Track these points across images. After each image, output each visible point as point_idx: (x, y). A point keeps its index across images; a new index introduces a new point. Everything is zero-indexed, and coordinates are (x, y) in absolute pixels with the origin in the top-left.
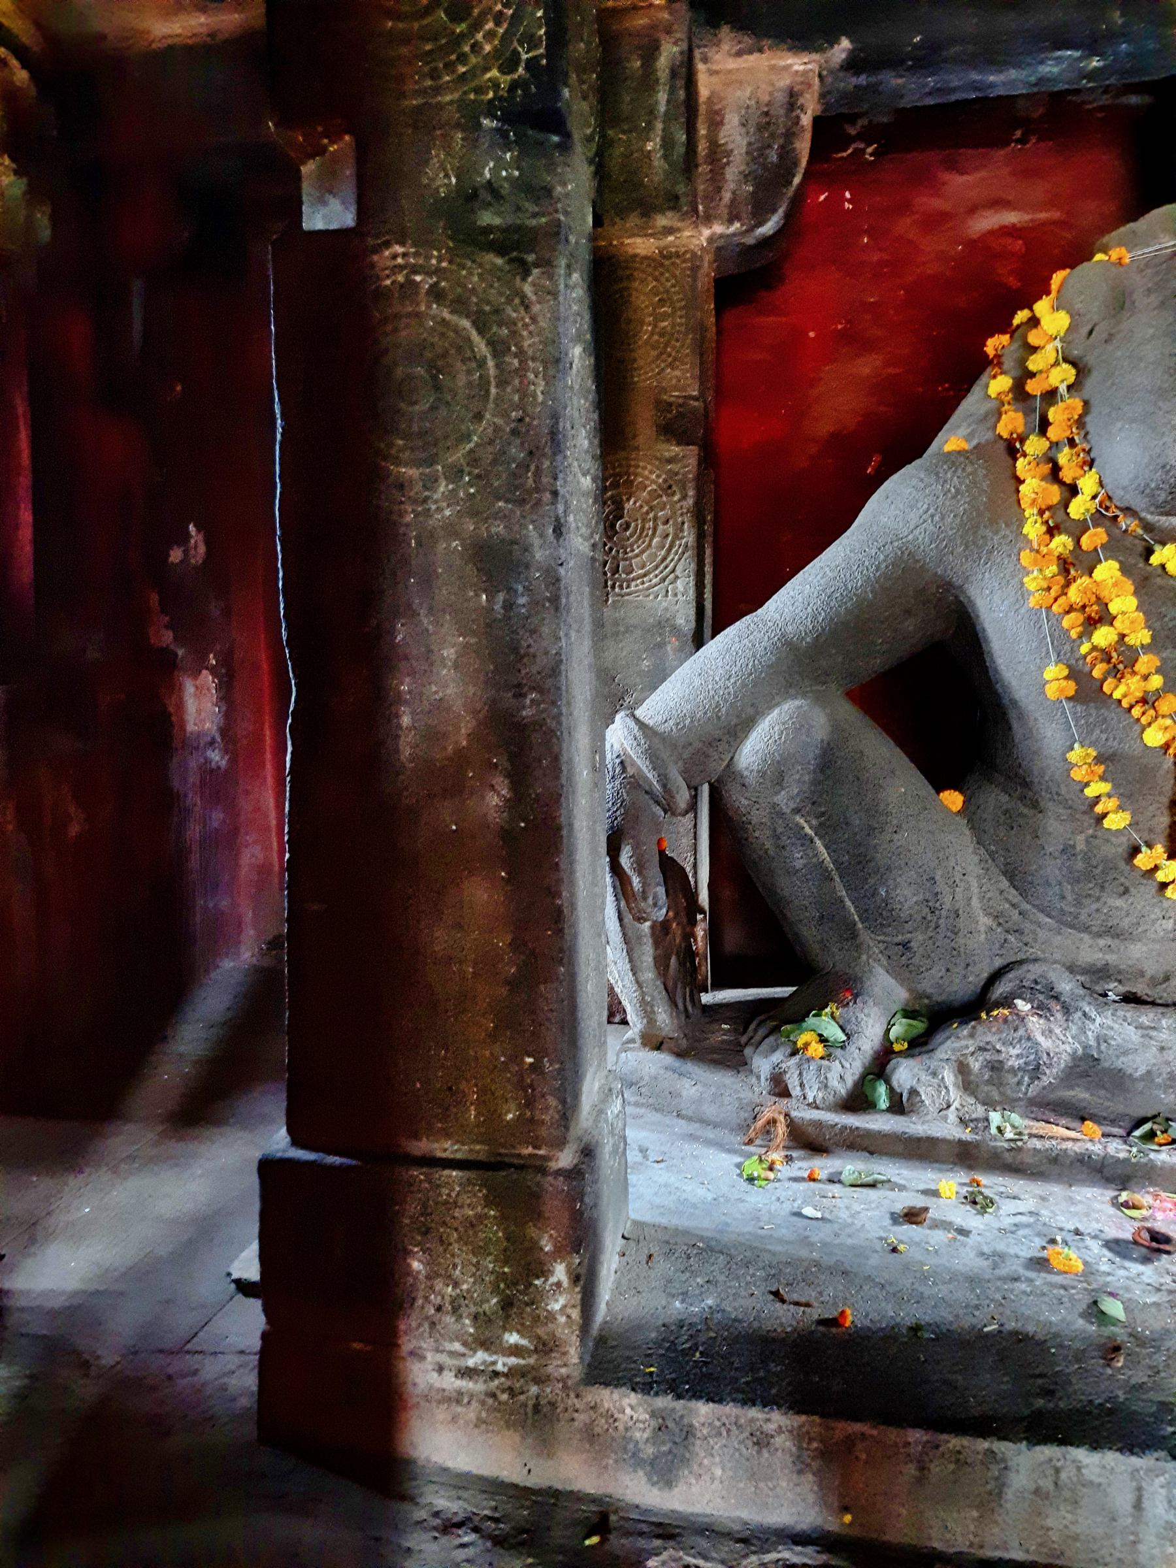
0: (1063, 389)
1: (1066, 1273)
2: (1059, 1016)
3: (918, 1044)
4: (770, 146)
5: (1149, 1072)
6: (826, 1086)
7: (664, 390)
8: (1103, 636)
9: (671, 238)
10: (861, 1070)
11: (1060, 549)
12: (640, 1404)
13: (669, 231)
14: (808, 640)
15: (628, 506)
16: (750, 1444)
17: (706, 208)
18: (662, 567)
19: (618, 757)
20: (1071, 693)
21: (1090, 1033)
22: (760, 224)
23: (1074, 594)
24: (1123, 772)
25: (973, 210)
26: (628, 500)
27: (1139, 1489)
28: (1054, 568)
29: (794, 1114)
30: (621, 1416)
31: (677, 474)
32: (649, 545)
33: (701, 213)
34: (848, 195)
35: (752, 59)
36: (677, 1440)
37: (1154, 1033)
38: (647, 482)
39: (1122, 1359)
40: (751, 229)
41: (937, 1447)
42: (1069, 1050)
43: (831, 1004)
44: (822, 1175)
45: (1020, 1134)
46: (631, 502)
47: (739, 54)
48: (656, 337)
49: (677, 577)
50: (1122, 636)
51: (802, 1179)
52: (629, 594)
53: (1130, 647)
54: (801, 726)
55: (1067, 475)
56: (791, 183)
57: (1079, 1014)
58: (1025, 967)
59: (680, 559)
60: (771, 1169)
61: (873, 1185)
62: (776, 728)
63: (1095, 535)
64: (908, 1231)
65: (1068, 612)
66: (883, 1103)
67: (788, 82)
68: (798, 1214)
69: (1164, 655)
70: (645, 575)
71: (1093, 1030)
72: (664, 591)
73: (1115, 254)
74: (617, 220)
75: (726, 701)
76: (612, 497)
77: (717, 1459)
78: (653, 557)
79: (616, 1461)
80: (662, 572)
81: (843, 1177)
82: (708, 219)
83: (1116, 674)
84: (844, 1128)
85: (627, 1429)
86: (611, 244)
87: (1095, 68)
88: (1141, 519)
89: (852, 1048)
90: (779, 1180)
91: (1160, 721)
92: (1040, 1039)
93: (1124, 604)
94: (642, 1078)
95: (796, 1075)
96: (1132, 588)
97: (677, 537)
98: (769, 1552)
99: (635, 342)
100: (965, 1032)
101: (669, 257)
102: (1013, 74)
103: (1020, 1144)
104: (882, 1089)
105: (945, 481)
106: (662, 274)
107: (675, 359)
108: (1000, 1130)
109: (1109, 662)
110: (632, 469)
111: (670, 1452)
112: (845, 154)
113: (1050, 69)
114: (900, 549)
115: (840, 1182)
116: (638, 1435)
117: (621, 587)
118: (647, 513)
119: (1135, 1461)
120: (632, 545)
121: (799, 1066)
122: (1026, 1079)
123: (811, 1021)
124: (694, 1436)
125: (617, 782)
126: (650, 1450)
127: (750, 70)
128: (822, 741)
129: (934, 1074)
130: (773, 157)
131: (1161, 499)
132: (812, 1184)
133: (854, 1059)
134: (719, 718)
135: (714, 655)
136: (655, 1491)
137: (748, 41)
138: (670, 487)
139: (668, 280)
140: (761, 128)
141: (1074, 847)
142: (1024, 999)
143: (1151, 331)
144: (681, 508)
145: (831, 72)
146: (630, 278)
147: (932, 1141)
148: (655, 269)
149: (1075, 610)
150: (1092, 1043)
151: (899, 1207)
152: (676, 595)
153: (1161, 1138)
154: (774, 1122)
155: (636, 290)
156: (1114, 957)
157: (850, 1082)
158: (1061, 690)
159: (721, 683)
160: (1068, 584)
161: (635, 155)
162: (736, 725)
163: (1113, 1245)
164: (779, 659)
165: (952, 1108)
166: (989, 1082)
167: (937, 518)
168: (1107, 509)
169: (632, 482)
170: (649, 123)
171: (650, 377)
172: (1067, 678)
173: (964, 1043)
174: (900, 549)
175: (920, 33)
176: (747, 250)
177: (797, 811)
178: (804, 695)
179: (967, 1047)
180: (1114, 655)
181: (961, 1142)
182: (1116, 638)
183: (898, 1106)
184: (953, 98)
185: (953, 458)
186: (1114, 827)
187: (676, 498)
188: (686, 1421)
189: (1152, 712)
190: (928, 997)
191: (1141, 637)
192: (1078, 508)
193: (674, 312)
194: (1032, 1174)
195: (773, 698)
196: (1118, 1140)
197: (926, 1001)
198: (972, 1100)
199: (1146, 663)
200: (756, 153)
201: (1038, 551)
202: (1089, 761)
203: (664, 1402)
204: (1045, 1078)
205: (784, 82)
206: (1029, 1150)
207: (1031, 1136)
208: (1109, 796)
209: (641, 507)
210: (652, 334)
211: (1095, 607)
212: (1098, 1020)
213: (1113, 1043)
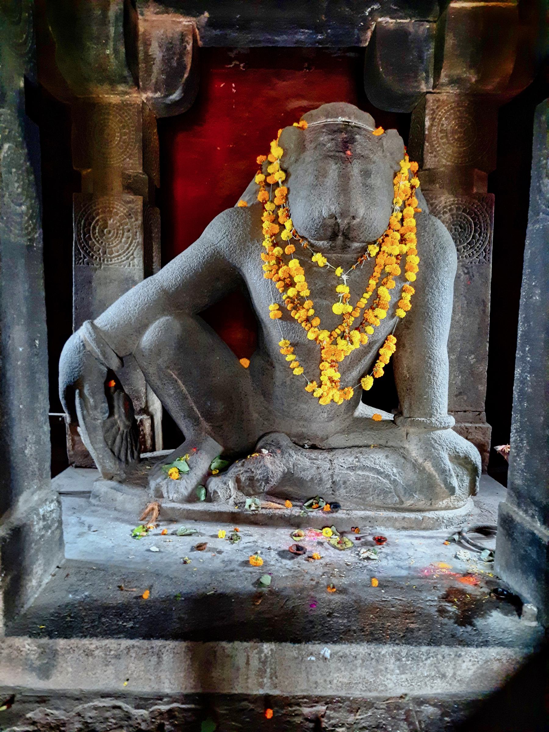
0: (280, 183)
1: (255, 566)
2: (279, 455)
3: (223, 470)
4: (173, 58)
5: (312, 478)
6: (178, 492)
7: (126, 169)
8: (291, 292)
9: (127, 97)
10: (196, 483)
11: (277, 253)
12: (32, 643)
13: (126, 93)
14: (173, 289)
15: (110, 222)
16: (83, 655)
17: (143, 84)
18: (127, 252)
19: (82, 342)
20: (280, 316)
21: (291, 463)
22: (171, 94)
23: (281, 274)
24: (301, 350)
25: (288, 97)
26: (110, 220)
27: (248, 656)
28: (274, 262)
29: (163, 505)
30: (24, 649)
31: (133, 209)
32: (121, 242)
33: (141, 86)
34: (233, 85)
35: (164, 17)
36: (51, 657)
37: (315, 461)
38: (118, 212)
39: (260, 601)
40: (167, 96)
41: (165, 647)
42: (282, 470)
43: (188, 455)
44: (170, 532)
45: (258, 507)
46: (112, 221)
47: (157, 13)
48: (121, 143)
49: (134, 258)
50: (299, 292)
51: (160, 534)
52: (111, 264)
53: (302, 297)
54: (167, 329)
55: (281, 220)
56: (183, 76)
57: (287, 454)
58: (270, 435)
59: (135, 249)
60: (147, 531)
61: (190, 535)
62: (157, 330)
63: (290, 247)
64: (197, 554)
65: (278, 281)
66: (203, 498)
67: (181, 29)
68: (149, 550)
69: (315, 301)
70: (119, 256)
71: (292, 461)
72: (128, 264)
73: (301, 124)
74: (99, 85)
75: (134, 316)
76: (102, 218)
77: (69, 664)
78: (122, 247)
79: (23, 670)
80: (127, 255)
81: (177, 532)
82: (145, 90)
83: (295, 308)
84: (184, 510)
85: (27, 654)
86: (98, 97)
87: (320, 39)
88: (309, 242)
89: (192, 474)
90: (148, 536)
91: (312, 329)
92: (269, 466)
93: (300, 278)
94: (101, 494)
95: (165, 488)
96: (303, 273)
97: (133, 239)
98: (89, 702)
99: (111, 145)
100: (240, 464)
101: (127, 105)
102: (285, 37)
103: (257, 512)
104: (203, 491)
105: (233, 220)
106: (123, 113)
107: (131, 154)
108: (250, 506)
109: (294, 304)
110: (111, 205)
111: (47, 663)
112: (231, 66)
113: (301, 37)
114: (214, 250)
115: (176, 534)
116: (32, 657)
117: (107, 261)
118: (119, 226)
119: (245, 644)
120: (112, 241)
121: (167, 483)
122: (263, 483)
123: (176, 463)
124: (58, 654)
125: (81, 354)
126: (38, 663)
127: (163, 22)
128: (178, 335)
129: (225, 484)
130: (175, 64)
131: (313, 233)
132: (163, 536)
133: (192, 479)
134: (131, 324)
135: (131, 295)
136: (41, 681)
137: (162, 8)
138: (130, 215)
139: (126, 116)
140: (168, 49)
141: (286, 382)
142: (266, 449)
143: (311, 159)
144: (135, 225)
145: (203, 27)
146: (108, 114)
147: (221, 513)
148: (120, 110)
149: (281, 280)
150: (291, 467)
151: (196, 544)
152: (134, 266)
153: (315, 506)
154: (153, 509)
155: (112, 120)
156: (306, 429)
157: (190, 489)
158: (275, 315)
159: (132, 308)
160: (279, 268)
161: (101, 56)
162: (139, 328)
163: (282, 554)
164: (159, 297)
165: (232, 498)
166: (249, 486)
167: (229, 237)
168: (295, 236)
169: (111, 211)
170: (106, 41)
171: (119, 163)
172: (278, 310)
173: (239, 469)
174: (214, 250)
175: (239, 14)
176: (169, 106)
177: (168, 367)
178: (171, 315)
179: (240, 471)
180: (296, 300)
181: (233, 513)
182: (297, 293)
183: (209, 499)
184: (261, 45)
185: (238, 210)
186: (297, 374)
187: (133, 220)
188: (54, 648)
189: (309, 325)
190: (232, 450)
191: (305, 293)
192: (285, 235)
193: (130, 132)
194: (262, 525)
195: (156, 316)
196: (298, 508)
197: (232, 451)
198: (241, 494)
199: (308, 304)
200: (166, 61)
201: (268, 254)
202: (287, 345)
203: (45, 640)
204: (271, 483)
205: (179, 29)
206: (260, 514)
207: (262, 508)
208: (296, 360)
209: (116, 223)
210: (120, 141)
211: (289, 280)
212: (295, 457)
213: (299, 466)
